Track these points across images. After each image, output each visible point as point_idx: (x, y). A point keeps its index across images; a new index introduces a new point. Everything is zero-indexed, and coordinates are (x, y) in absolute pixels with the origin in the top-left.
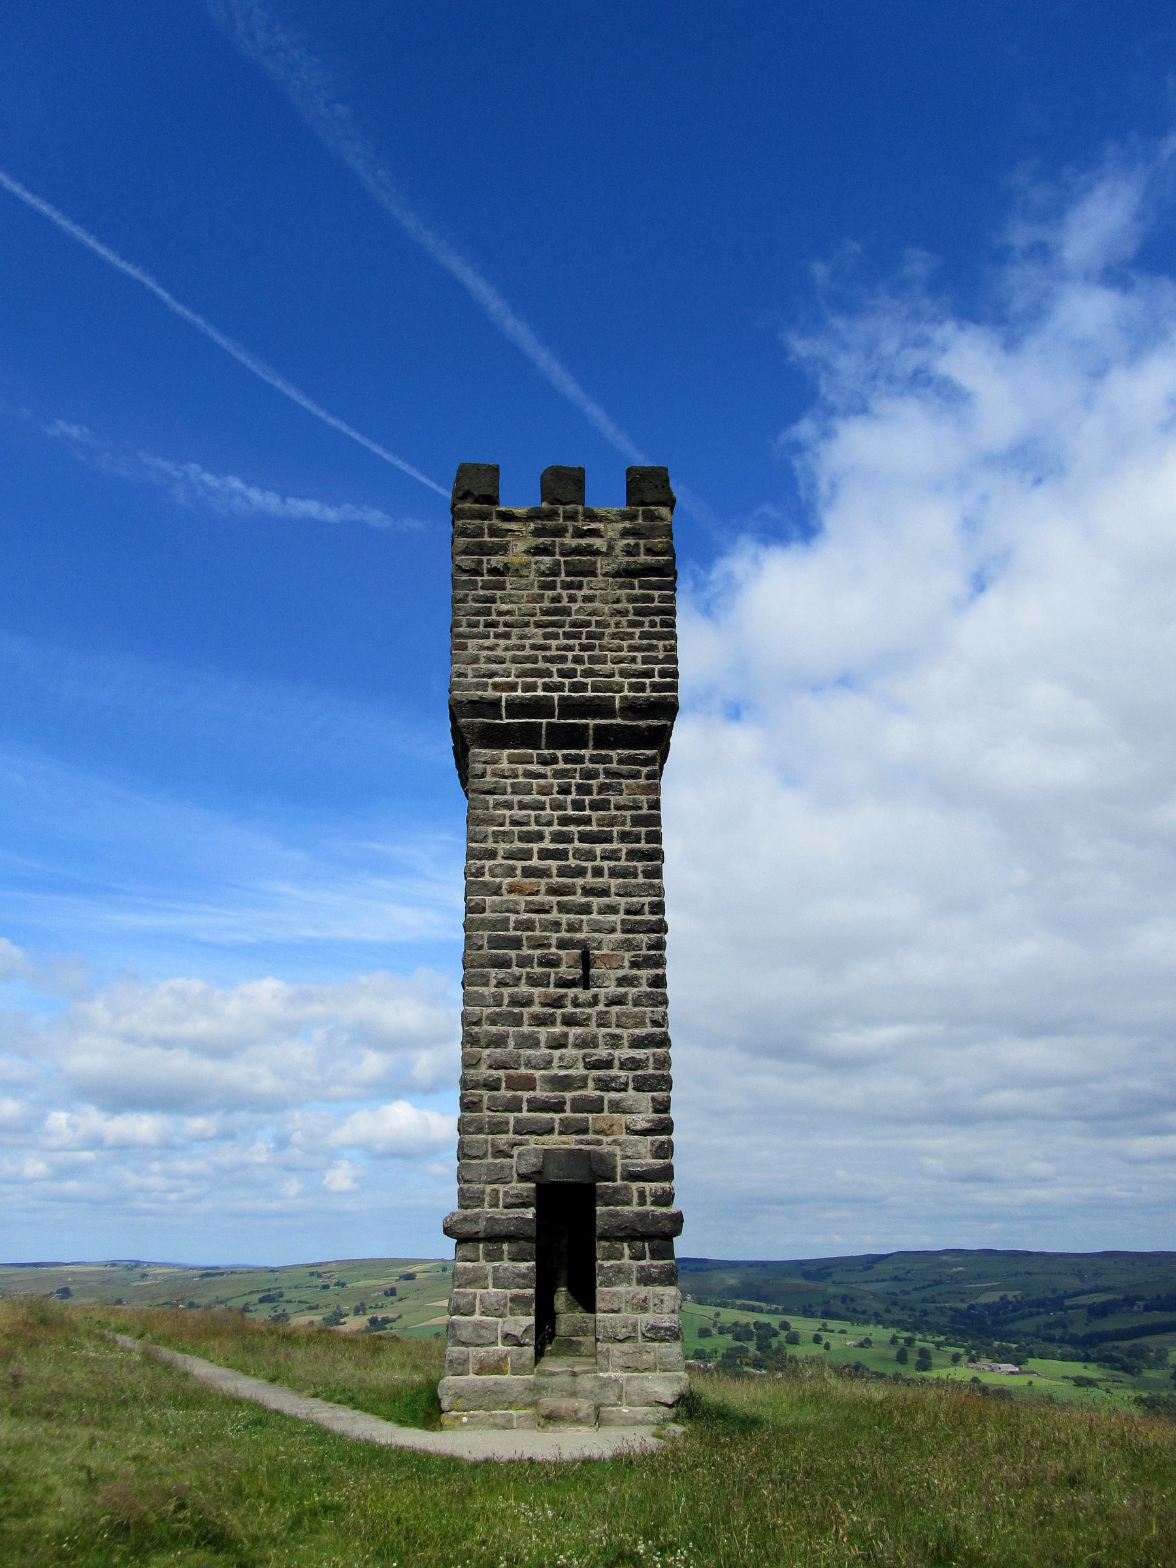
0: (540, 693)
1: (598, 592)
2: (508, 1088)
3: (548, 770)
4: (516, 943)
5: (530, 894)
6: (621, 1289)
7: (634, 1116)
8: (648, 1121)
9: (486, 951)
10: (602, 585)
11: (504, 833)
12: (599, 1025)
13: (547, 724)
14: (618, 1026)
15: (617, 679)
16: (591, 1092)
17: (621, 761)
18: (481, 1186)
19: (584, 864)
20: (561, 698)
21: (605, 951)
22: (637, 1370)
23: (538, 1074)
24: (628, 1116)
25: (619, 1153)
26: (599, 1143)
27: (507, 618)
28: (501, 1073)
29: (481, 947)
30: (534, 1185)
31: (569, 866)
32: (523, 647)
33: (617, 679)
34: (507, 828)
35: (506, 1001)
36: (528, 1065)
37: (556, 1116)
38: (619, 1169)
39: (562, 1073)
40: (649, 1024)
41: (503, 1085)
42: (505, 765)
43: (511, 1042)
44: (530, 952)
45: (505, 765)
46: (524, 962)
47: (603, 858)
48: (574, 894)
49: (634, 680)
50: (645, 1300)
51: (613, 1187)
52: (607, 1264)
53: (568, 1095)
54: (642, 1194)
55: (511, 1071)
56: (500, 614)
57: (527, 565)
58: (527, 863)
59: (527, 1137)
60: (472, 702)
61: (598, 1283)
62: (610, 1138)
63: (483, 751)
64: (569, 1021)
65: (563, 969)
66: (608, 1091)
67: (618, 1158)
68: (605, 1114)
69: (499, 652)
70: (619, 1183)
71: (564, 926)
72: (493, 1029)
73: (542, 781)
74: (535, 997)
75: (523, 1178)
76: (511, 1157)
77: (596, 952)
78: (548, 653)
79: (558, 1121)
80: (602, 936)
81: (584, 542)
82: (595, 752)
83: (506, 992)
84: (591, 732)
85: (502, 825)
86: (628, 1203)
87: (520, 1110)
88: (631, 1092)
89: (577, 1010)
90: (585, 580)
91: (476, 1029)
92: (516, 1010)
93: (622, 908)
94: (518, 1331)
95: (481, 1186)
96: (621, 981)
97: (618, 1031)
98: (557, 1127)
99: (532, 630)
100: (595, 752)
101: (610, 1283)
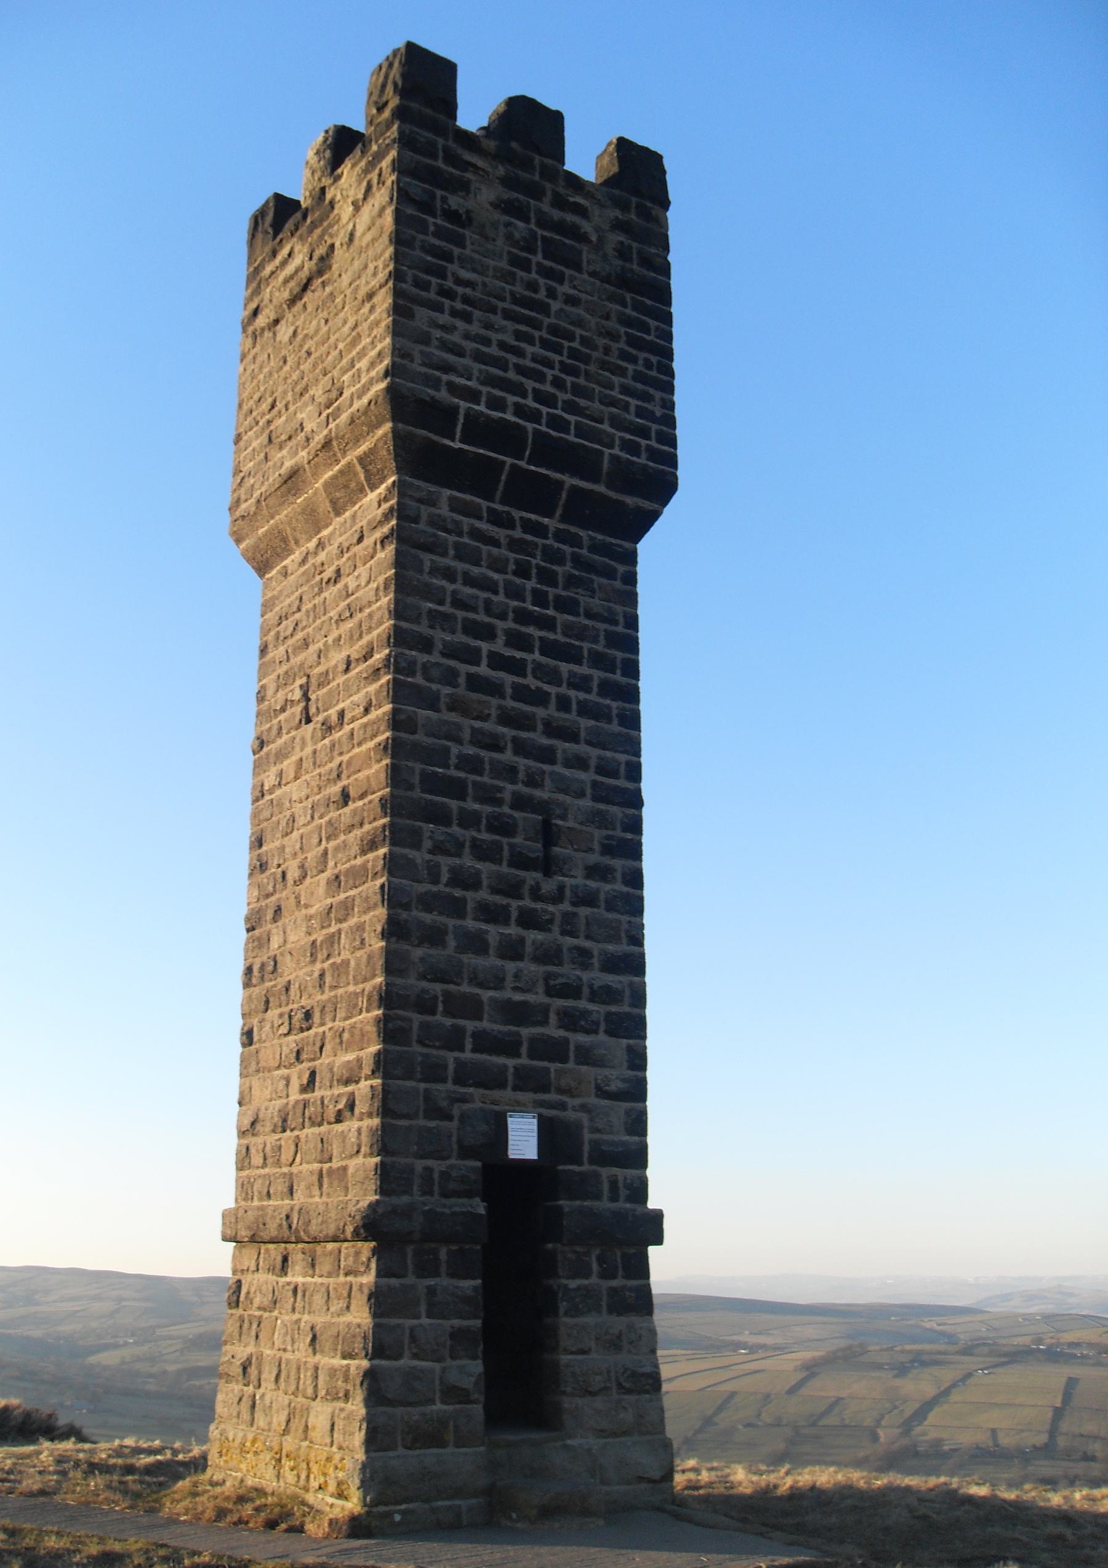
0: (509, 417)
1: (583, 296)
2: (448, 1013)
3: (501, 533)
4: (457, 789)
5: (477, 718)
6: (590, 1320)
7: (606, 1072)
8: (624, 1080)
9: (417, 793)
10: (589, 288)
11: (445, 616)
12: (564, 933)
13: (513, 466)
14: (587, 937)
15: (606, 427)
16: (552, 1030)
17: (594, 548)
18: (409, 1160)
19: (546, 687)
20: (536, 432)
21: (570, 824)
22: (615, 1434)
23: (487, 995)
24: (599, 1071)
25: (586, 1123)
26: (563, 1106)
27: (468, 291)
28: (437, 988)
29: (411, 787)
30: (479, 1164)
31: (527, 687)
32: (487, 342)
33: (606, 427)
34: (446, 608)
35: (445, 877)
36: (474, 980)
37: (511, 1062)
38: (586, 1148)
39: (518, 997)
40: (624, 940)
41: (440, 1008)
42: (444, 510)
43: (452, 943)
44: (477, 806)
45: (444, 510)
46: (469, 820)
47: (571, 685)
48: (533, 729)
49: (628, 436)
50: (619, 1337)
51: (580, 1173)
52: (573, 1284)
53: (526, 1032)
54: (614, 1184)
55: (451, 987)
56: (459, 282)
57: (495, 225)
58: (473, 669)
59: (471, 1090)
60: (422, 402)
61: (562, 1311)
62: (577, 1102)
63: (417, 482)
64: (528, 920)
65: (518, 840)
66: (575, 1031)
67: (586, 1131)
68: (571, 1065)
69: (456, 338)
70: (586, 1167)
71: (521, 776)
72: (428, 918)
73: (495, 551)
74: (484, 876)
75: (466, 1152)
76: (450, 1118)
77: (560, 822)
78: (521, 361)
79: (511, 1070)
80: (568, 799)
81: (570, 218)
82: (562, 526)
83: (446, 863)
84: (564, 495)
85: (441, 602)
86: (598, 1197)
87: (462, 1049)
88: (602, 1037)
89: (539, 906)
90: (568, 272)
91: (404, 915)
92: (458, 893)
93: (593, 763)
94: (467, 1383)
95: (409, 1160)
96: (593, 871)
97: (587, 944)
98: (510, 1078)
99: (498, 320)
100: (562, 526)
101: (574, 1311)
